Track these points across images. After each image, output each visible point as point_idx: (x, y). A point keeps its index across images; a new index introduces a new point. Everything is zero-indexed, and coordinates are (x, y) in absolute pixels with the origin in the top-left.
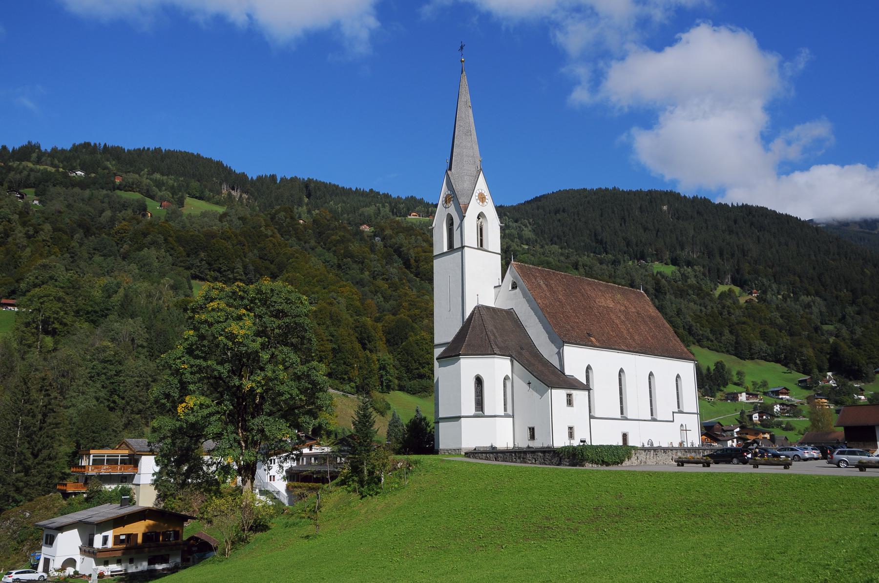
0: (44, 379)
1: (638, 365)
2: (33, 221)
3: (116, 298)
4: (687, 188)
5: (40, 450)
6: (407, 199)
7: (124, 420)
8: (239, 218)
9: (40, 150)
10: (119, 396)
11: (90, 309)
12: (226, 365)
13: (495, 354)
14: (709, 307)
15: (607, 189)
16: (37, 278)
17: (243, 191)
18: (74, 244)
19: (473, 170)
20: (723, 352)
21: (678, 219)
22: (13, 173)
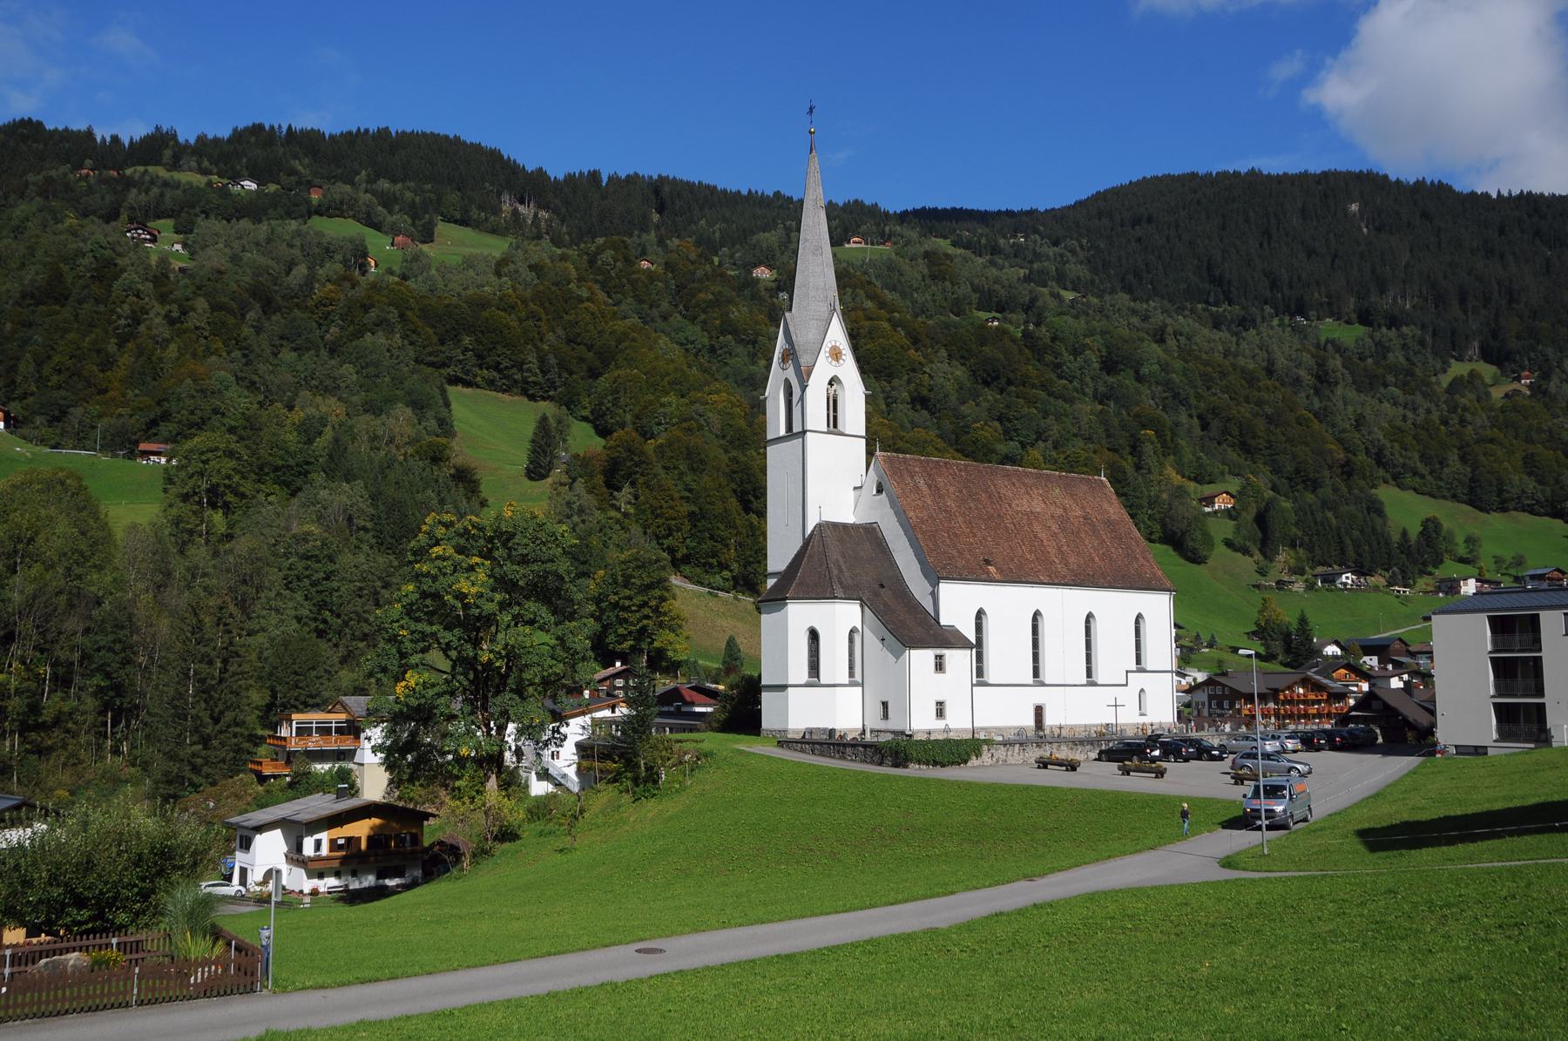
0: (221, 608)
1: (1064, 606)
2: (178, 294)
3: (322, 443)
4: (1403, 162)
5: (222, 713)
6: (847, 205)
7: (342, 651)
8: (530, 267)
9: (176, 141)
10: (331, 611)
11: (280, 463)
12: (456, 631)
14: (1421, 410)
16: (192, 413)
17: (540, 206)
18: (246, 331)
19: (823, 309)
20: (1444, 497)
21: (1379, 229)
22: (134, 191)
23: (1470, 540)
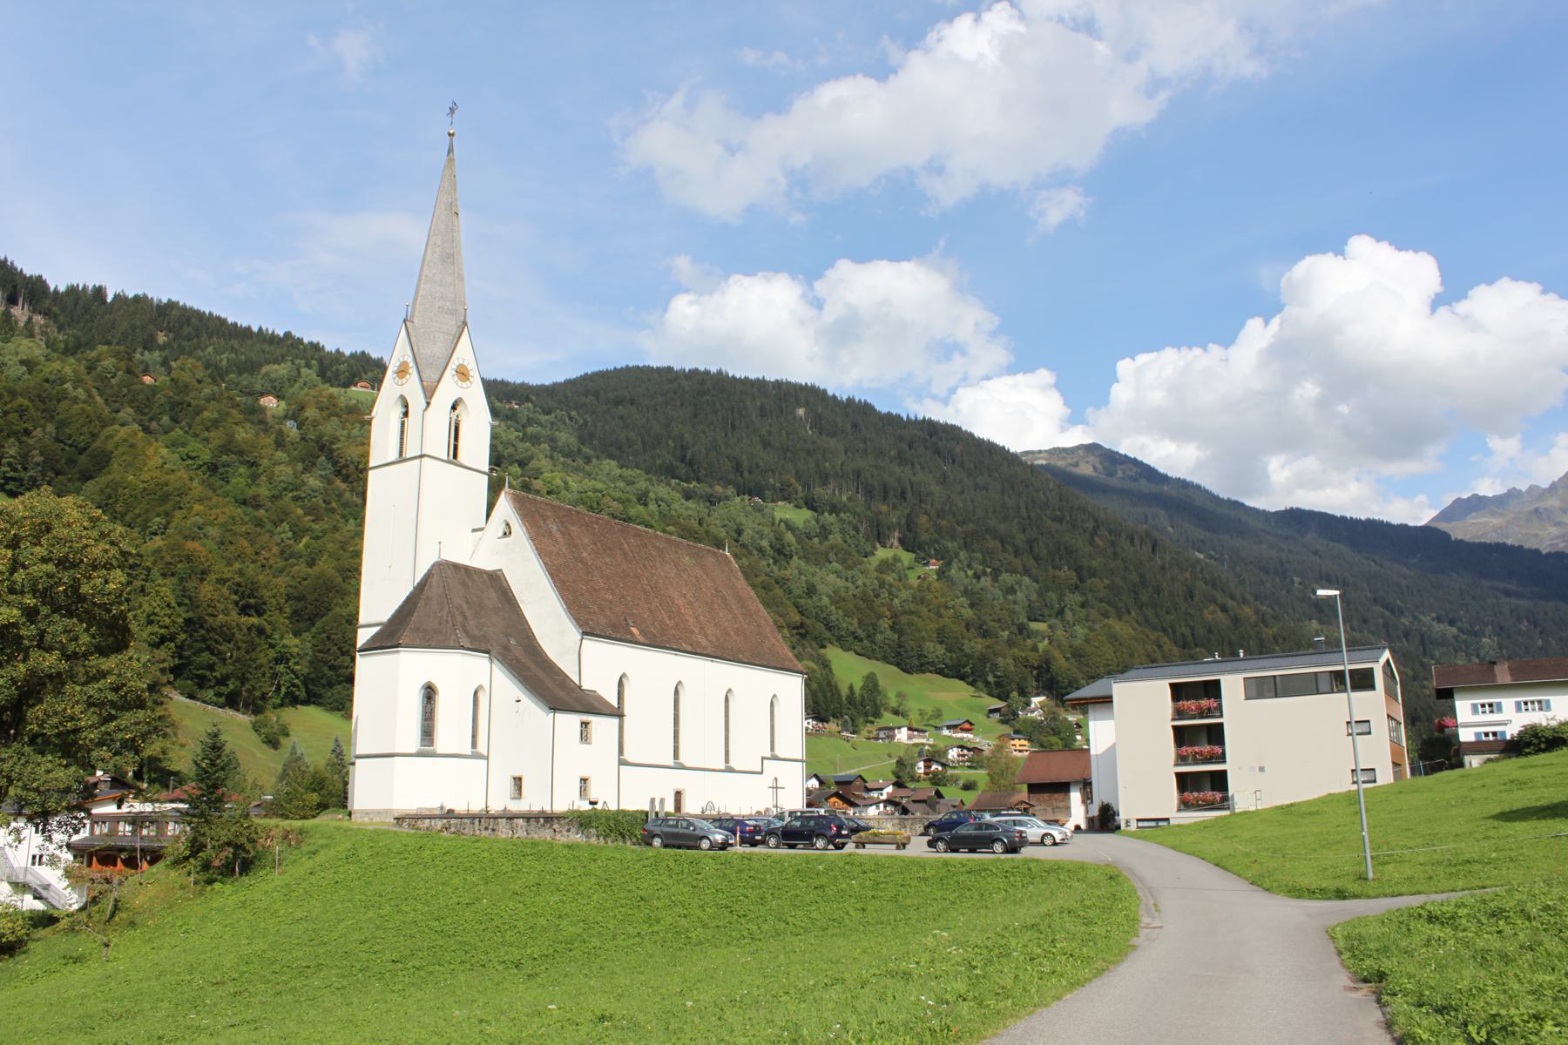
1: (707, 678)
6: (353, 356)
8: (22, 362)
13: (462, 647)
15: (707, 372)
23: (900, 695)
